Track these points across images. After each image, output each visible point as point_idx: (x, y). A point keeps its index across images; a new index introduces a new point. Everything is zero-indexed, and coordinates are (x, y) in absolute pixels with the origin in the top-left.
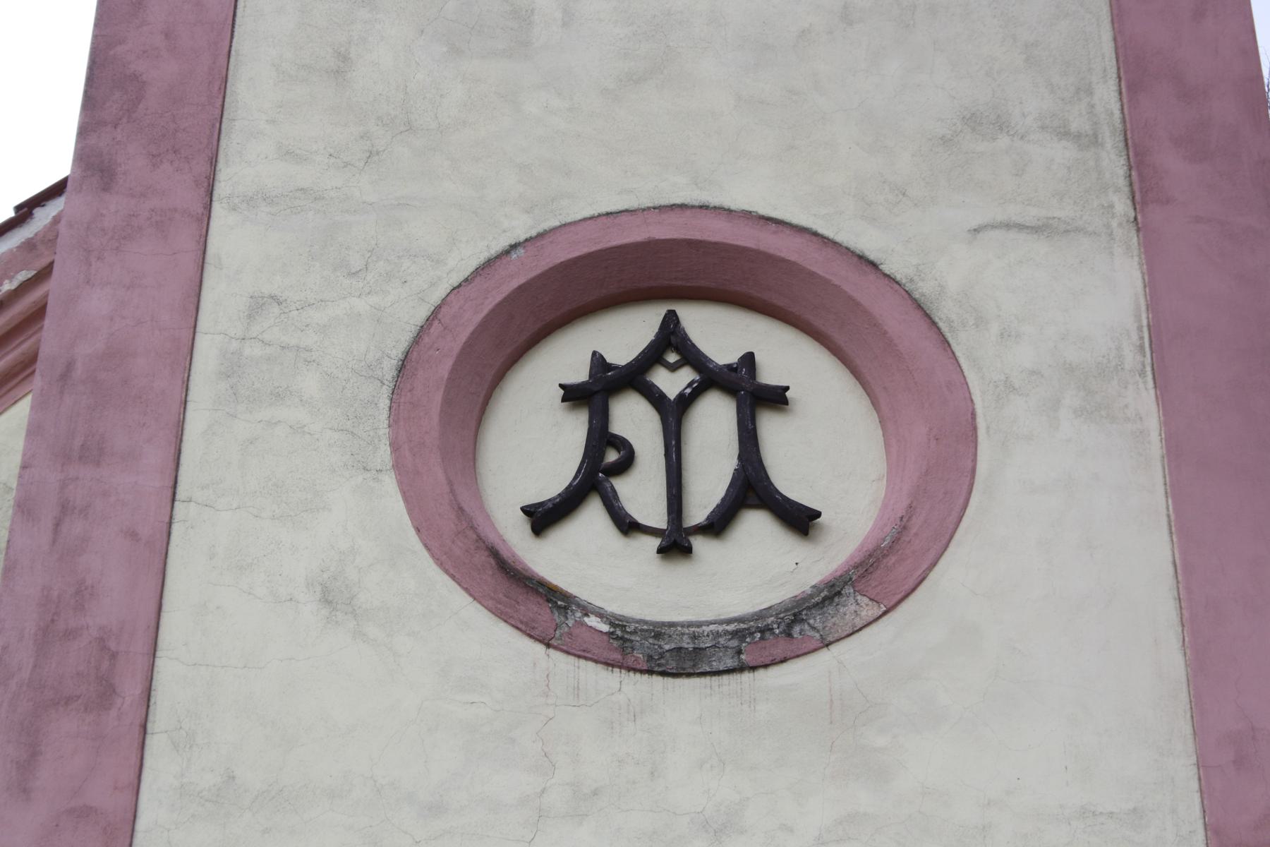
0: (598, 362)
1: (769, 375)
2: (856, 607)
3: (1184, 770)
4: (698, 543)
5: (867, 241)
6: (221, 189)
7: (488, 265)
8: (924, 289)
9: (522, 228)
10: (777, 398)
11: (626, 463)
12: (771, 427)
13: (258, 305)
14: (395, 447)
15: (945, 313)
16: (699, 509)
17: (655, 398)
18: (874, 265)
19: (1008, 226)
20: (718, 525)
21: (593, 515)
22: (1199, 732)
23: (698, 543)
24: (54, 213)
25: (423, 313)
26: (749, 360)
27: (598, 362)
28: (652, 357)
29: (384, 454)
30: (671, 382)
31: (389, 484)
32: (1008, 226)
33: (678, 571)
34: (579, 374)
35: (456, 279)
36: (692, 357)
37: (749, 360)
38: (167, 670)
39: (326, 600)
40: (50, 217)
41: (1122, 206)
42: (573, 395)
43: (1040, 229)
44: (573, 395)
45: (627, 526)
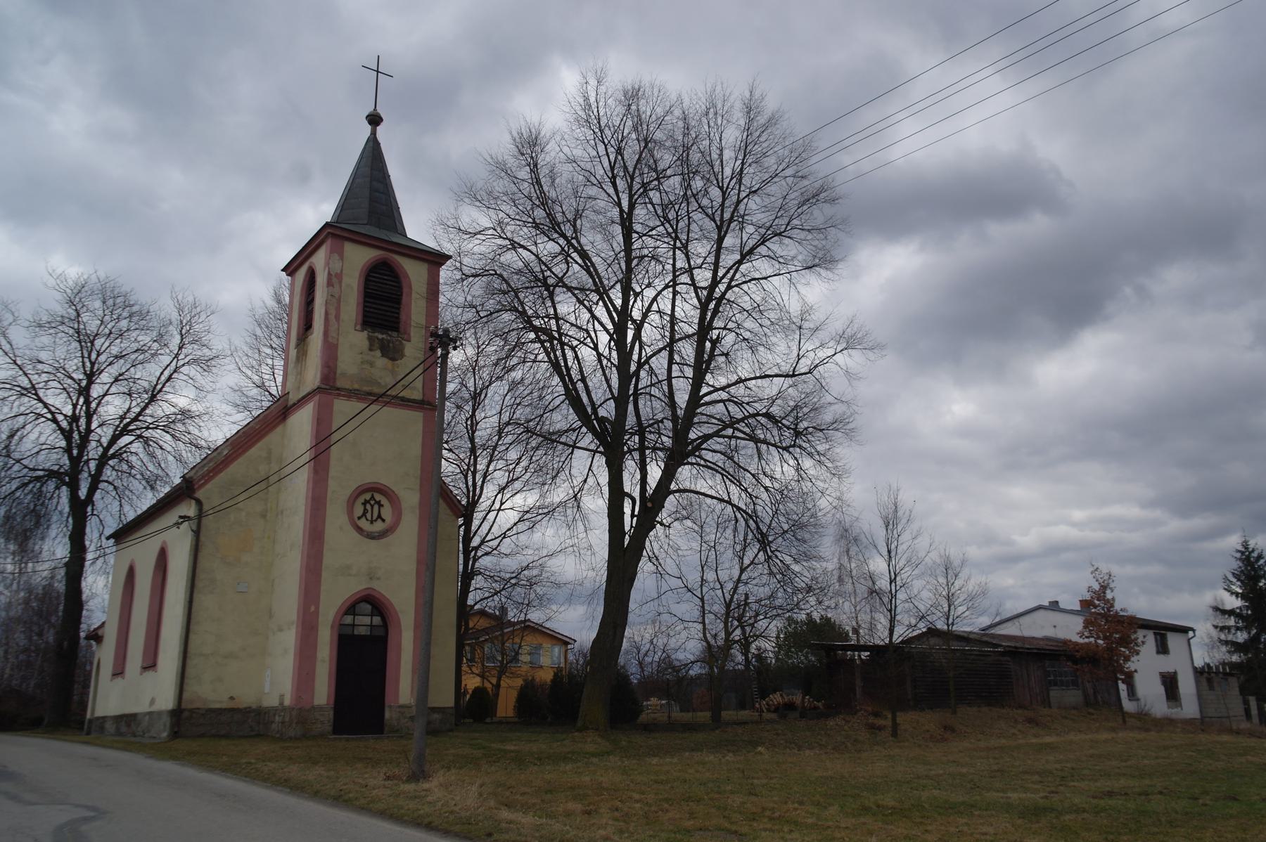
1: (382, 503)
2: (389, 533)
5: (394, 489)
10: (382, 506)
12: (382, 508)
16: (374, 518)
20: (376, 520)
28: (371, 499)
30: (372, 502)
34: (363, 501)
45: (367, 520)
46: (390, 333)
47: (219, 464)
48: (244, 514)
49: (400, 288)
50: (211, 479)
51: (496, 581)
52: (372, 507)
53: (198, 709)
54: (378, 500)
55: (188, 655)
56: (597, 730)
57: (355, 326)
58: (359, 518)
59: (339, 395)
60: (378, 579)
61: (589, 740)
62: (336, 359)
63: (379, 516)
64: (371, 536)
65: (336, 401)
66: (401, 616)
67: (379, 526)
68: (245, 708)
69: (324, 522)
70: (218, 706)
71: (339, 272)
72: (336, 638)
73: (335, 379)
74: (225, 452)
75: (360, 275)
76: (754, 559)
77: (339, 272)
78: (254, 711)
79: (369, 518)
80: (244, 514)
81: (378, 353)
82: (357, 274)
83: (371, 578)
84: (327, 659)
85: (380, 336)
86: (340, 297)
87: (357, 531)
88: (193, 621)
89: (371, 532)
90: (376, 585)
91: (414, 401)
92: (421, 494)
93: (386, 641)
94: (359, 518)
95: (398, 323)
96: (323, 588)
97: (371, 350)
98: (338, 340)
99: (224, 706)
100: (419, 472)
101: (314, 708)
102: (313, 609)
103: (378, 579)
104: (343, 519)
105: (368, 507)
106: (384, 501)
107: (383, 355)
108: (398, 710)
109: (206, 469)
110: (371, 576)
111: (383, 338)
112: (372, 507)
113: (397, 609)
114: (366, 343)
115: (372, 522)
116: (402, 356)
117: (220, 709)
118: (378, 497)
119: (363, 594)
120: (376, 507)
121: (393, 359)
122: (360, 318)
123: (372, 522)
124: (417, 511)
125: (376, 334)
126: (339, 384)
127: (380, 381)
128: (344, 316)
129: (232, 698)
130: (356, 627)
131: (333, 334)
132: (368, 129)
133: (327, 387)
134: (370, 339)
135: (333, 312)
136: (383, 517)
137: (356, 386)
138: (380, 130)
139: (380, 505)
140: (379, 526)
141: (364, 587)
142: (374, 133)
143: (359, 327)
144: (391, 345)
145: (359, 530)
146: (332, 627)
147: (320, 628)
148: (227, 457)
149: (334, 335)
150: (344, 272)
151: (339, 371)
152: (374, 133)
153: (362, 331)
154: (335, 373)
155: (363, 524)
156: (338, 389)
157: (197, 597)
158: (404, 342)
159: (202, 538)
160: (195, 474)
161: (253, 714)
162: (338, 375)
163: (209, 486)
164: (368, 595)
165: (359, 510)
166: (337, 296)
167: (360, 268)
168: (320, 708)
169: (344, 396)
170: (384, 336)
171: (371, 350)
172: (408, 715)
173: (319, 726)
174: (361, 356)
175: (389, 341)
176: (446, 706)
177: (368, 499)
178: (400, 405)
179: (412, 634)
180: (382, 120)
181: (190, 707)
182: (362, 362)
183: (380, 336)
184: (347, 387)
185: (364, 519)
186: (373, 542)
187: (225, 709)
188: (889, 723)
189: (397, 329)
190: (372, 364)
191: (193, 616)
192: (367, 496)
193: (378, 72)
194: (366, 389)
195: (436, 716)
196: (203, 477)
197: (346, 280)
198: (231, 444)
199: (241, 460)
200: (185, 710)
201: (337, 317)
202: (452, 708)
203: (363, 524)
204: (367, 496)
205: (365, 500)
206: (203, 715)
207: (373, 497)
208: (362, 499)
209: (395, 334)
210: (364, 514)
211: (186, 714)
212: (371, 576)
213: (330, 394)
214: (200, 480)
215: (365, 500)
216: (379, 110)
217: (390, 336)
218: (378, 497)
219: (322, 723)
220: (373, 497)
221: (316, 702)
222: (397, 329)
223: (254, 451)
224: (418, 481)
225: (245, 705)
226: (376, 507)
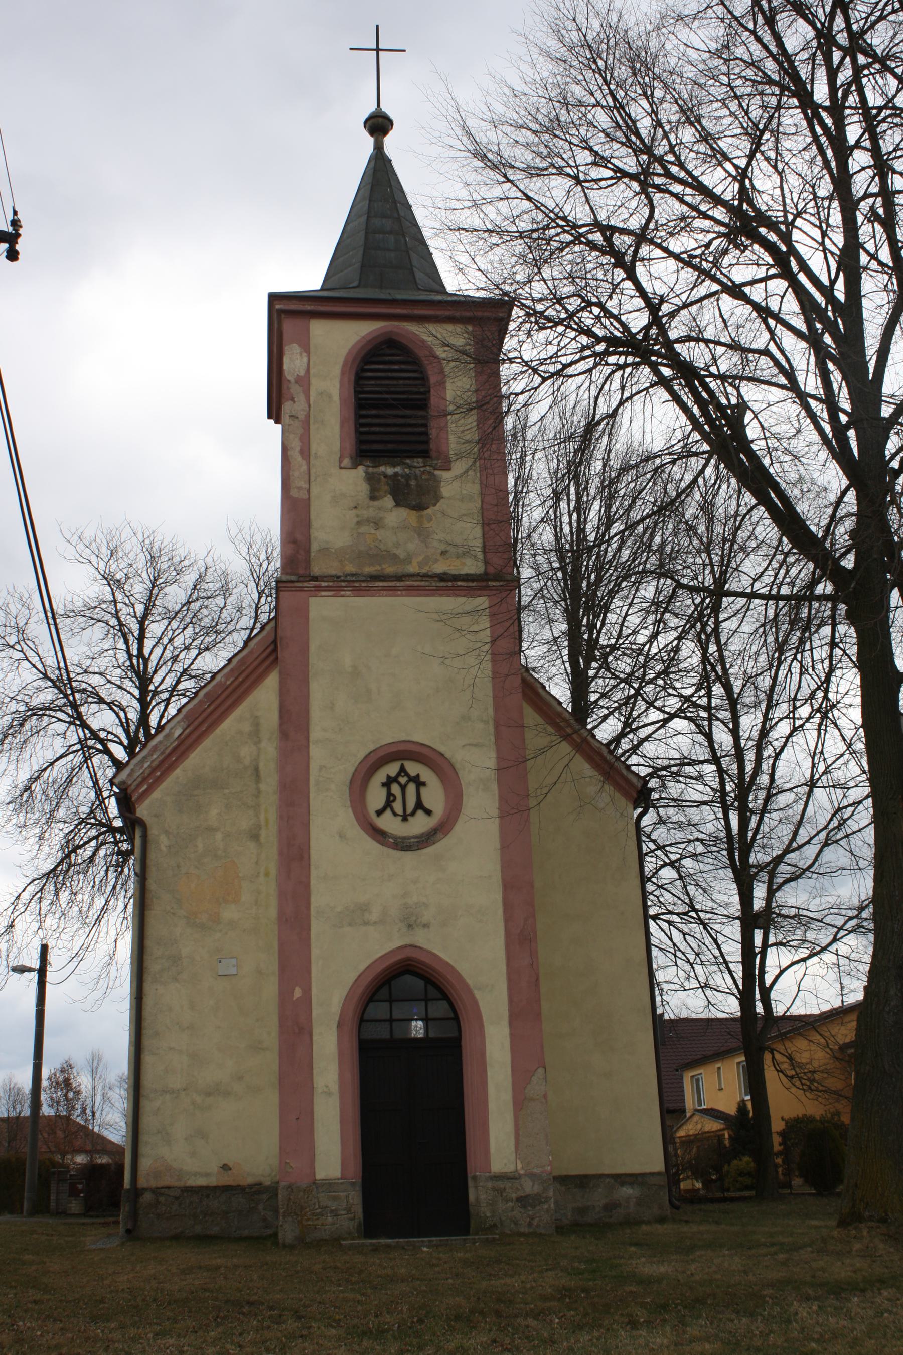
0: (388, 777)
1: (422, 779)
2: (439, 835)
3: (498, 867)
4: (409, 818)
5: (442, 749)
6: (311, 739)
7: (366, 757)
8: (453, 761)
9: (372, 747)
10: (424, 784)
11: (394, 800)
12: (423, 790)
13: (321, 768)
14: (351, 801)
15: (457, 766)
16: (409, 810)
17: (399, 784)
18: (443, 755)
19: (470, 745)
20: (413, 814)
21: (388, 812)
22: (501, 860)
23: (409, 818)
24: (659, 1226)
25: (353, 769)
26: (418, 776)
27: (388, 777)
28: (399, 775)
29: (348, 803)
30: (403, 780)
31: (350, 810)
32: (470, 745)
33: (405, 824)
34: (384, 780)
35: (359, 761)
36: (407, 774)
37: (418, 776)
38: (312, 852)
39: (340, 836)
40: (665, 1226)
41: (493, 739)
42: (384, 785)
43: (475, 745)
44: (384, 785)
45: (395, 814)
46: (408, 461)
47: (170, 754)
48: (219, 836)
49: (424, 379)
50: (158, 781)
51: (73, 770)
52: (403, 788)
53: (169, 1188)
54: (413, 773)
55: (143, 1091)
56: (884, 1220)
57: (340, 462)
58: (379, 813)
59: (318, 589)
60: (426, 926)
61: (857, 1246)
62: (307, 525)
63: (419, 805)
64: (403, 845)
65: (313, 601)
66: (478, 994)
67: (419, 824)
68: (251, 1186)
69: (306, 826)
70: (201, 1182)
71: (302, 373)
72: (352, 1047)
73: (308, 562)
74: (177, 733)
75: (343, 373)
76: (754, 351)
77: (302, 373)
78: (267, 1189)
79: (399, 810)
80: (219, 836)
81: (388, 502)
82: (337, 370)
83: (410, 926)
84: (334, 1087)
85: (390, 471)
86: (308, 416)
87: (374, 838)
88: (147, 1032)
89: (404, 838)
90: (421, 939)
91: (467, 578)
92: (498, 751)
93: (460, 1047)
94: (379, 813)
95: (427, 442)
96: (315, 952)
97: (373, 498)
98: (308, 491)
99: (213, 1181)
100: (491, 711)
101: (315, 1184)
102: (298, 993)
103: (426, 926)
104: (345, 818)
105: (395, 789)
106: (426, 774)
107: (398, 504)
108: (490, 1185)
109: (146, 765)
110: (411, 923)
111: (396, 474)
112: (403, 788)
113: (470, 982)
114: (364, 488)
115: (405, 818)
116: (437, 498)
117: (207, 1188)
118: (413, 768)
119: (399, 957)
120: (411, 788)
121: (419, 507)
122: (350, 445)
123: (405, 818)
124: (495, 787)
125: (382, 469)
126: (316, 570)
127: (395, 551)
128: (316, 447)
129: (225, 1167)
130: (394, 1024)
131: (299, 482)
132: (368, 143)
133: (294, 578)
134: (370, 478)
135: (296, 445)
136: (427, 805)
137: (350, 568)
138: (390, 143)
139: (419, 783)
140: (419, 824)
141: (397, 943)
142: (379, 148)
143: (347, 462)
144: (413, 483)
145: (379, 834)
146: (340, 1025)
147: (315, 1031)
148: (181, 740)
149: (303, 484)
150: (312, 372)
151: (315, 547)
152: (379, 148)
153: (355, 466)
154: (308, 551)
155: (389, 823)
156: (315, 579)
157: (148, 987)
158: (437, 472)
159: (152, 884)
160: (130, 775)
161: (265, 1197)
162: (312, 554)
163: (156, 795)
164: (409, 959)
165: (376, 797)
166: (302, 416)
167: (341, 361)
168: (329, 1185)
169: (327, 589)
170: (398, 469)
171: (373, 498)
172: (514, 1196)
173: (330, 1219)
174: (354, 511)
175: (407, 477)
176: (648, 1171)
177: (393, 774)
178: (439, 589)
179: (506, 1031)
180: (391, 123)
181: (153, 1184)
182: (358, 523)
183: (390, 471)
184: (333, 572)
185: (388, 813)
186: (408, 856)
187: (215, 1188)
188: (713, 701)
189: (425, 454)
190: (377, 524)
191: (145, 1024)
192: (392, 769)
193: (378, 50)
194: (368, 570)
195: (627, 1191)
196: (145, 780)
197: (316, 385)
198: (186, 717)
199: (207, 742)
200: (144, 1190)
201: (306, 452)
202: (659, 1174)
203: (389, 823)
204: (392, 769)
205: (388, 777)
206: (177, 1198)
207: (402, 770)
208: (381, 776)
209: (418, 462)
210: (389, 804)
211: (147, 1197)
212: (411, 923)
213: (301, 589)
214: (140, 785)
215: (388, 777)
216: (384, 108)
217: (410, 467)
218: (413, 768)
219: (334, 1212)
220: (402, 770)
221: (320, 1175)
222: (425, 454)
223: (229, 725)
224: (491, 728)
225: (250, 1180)
226: (411, 788)
